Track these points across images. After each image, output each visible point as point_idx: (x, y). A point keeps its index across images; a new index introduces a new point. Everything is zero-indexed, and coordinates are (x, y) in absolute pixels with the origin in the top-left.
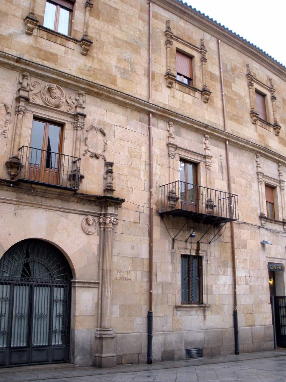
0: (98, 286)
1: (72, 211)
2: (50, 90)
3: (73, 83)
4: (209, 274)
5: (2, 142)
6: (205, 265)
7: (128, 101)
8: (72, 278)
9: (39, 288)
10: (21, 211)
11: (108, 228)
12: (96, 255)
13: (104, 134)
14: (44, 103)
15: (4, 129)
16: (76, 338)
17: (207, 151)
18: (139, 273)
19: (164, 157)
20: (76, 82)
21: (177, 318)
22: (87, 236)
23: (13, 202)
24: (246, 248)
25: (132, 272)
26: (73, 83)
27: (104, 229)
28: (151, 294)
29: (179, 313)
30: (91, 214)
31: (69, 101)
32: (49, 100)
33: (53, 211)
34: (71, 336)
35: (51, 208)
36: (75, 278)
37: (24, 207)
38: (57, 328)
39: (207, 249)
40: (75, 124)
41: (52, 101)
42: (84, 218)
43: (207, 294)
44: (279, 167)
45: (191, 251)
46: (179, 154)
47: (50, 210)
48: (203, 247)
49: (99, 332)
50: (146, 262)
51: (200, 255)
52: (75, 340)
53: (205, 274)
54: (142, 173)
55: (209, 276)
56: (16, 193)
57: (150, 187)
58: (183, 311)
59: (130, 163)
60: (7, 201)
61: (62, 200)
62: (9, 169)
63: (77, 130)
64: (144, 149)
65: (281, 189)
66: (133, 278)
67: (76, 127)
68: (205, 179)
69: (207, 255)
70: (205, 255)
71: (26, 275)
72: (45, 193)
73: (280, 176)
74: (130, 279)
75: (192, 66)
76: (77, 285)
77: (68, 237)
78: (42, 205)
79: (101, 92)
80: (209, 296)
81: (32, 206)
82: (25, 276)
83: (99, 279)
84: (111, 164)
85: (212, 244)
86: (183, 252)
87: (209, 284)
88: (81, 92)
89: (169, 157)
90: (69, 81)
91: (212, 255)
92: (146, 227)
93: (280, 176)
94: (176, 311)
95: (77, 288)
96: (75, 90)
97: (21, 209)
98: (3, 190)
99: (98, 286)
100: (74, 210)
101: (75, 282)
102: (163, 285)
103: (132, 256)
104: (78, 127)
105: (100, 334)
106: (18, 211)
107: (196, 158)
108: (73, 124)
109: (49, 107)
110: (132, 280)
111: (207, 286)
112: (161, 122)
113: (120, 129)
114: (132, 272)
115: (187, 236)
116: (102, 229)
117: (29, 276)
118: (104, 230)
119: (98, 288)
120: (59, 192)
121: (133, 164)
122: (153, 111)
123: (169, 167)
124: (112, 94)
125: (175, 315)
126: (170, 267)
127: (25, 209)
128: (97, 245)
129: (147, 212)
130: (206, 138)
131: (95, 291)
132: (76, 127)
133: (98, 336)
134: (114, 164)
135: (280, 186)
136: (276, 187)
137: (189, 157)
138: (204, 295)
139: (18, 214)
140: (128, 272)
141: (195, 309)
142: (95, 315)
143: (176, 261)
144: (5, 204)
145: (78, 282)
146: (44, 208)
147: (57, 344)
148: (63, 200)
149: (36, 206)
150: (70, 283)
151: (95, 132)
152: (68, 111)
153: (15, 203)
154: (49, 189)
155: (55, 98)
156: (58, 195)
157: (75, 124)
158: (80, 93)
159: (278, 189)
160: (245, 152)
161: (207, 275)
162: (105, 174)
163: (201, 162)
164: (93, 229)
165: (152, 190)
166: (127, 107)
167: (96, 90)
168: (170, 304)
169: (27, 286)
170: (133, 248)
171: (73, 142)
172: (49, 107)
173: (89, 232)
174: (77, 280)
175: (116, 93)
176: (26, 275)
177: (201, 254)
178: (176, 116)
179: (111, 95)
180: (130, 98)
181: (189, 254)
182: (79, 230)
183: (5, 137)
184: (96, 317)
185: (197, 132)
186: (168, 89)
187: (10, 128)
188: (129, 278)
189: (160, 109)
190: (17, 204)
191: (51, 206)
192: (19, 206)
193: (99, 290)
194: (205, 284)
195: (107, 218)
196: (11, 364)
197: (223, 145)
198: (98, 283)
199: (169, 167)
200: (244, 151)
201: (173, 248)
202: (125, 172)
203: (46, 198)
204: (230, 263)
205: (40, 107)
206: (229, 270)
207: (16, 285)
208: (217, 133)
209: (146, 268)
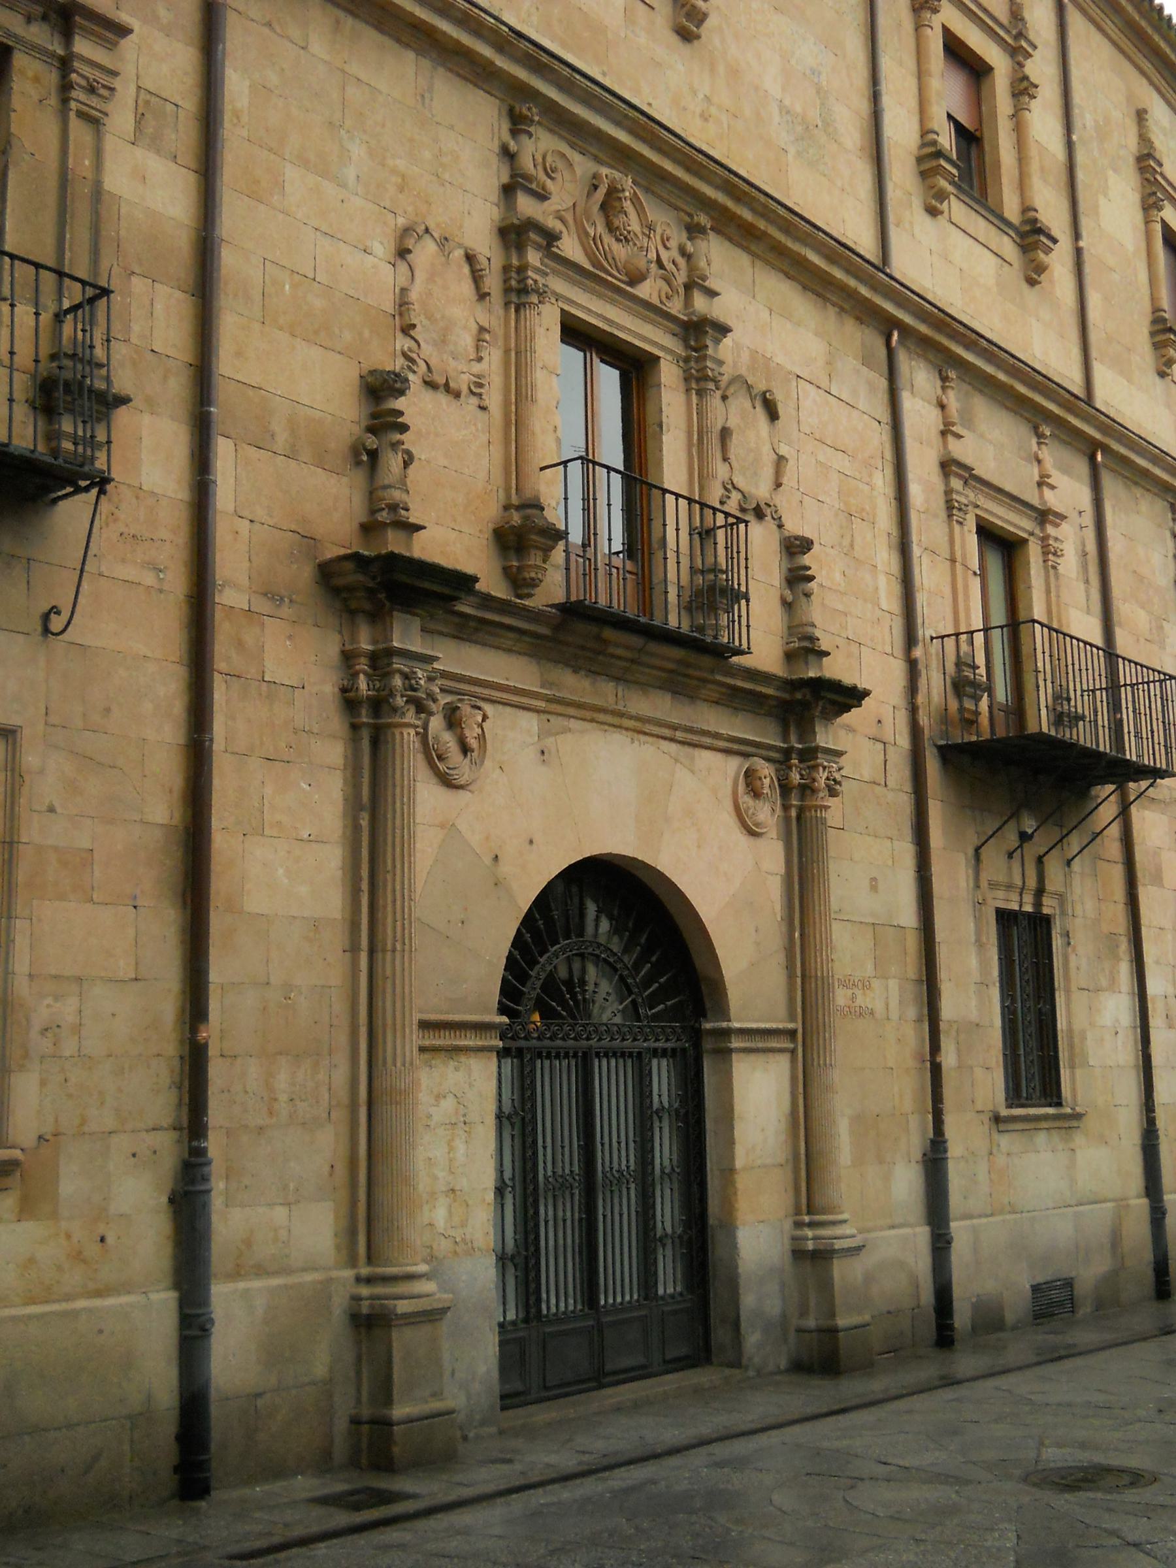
0: (792, 1046)
1: (708, 741)
2: (610, 205)
3: (679, 173)
4: (1074, 988)
5: (473, 428)
6: (1060, 950)
7: (838, 274)
8: (705, 1016)
9: (625, 1061)
10: (560, 738)
11: (816, 807)
12: (779, 919)
13: (772, 412)
14: (587, 254)
15: (477, 368)
16: (740, 1263)
17: (1046, 490)
18: (893, 984)
19: (936, 516)
20: (688, 169)
21: (1001, 1160)
22: (751, 839)
23: (505, 696)
24: (1161, 885)
25: (876, 984)
26: (679, 173)
27: (801, 810)
28: (936, 1070)
29: (1004, 1141)
30: (764, 752)
31: (665, 256)
32: (606, 247)
33: (650, 739)
34: (718, 1252)
35: (648, 728)
36: (724, 1014)
37: (565, 722)
38: (669, 1230)
39: (1063, 890)
40: (692, 364)
41: (620, 251)
42: (740, 767)
43: (1072, 1067)
44: (944, 388)
45: (1021, 895)
46: (977, 506)
47: (642, 738)
48: (1054, 882)
49: (365, 1291)
50: (912, 942)
51: (1045, 911)
52: (740, 1270)
53: (1062, 985)
54: (882, 581)
55: (1076, 995)
56: (538, 663)
57: (910, 638)
58: (1014, 1135)
59: (847, 542)
60: (515, 699)
61: (675, 693)
62: (512, 553)
63: (701, 393)
64: (882, 482)
65: (1045, 553)
66: (879, 1007)
67: (698, 380)
68: (1044, 606)
69: (1063, 913)
70: (1058, 912)
71: (564, 1013)
72: (632, 661)
73: (1045, 489)
74: (872, 1013)
75: (1149, 270)
76: (736, 1043)
77: (699, 847)
78: (621, 715)
79: (762, 224)
80: (1078, 1072)
81: (592, 720)
82: (563, 1018)
83: (792, 1017)
84: (805, 545)
85: (1076, 865)
86: (1002, 905)
87: (1077, 1026)
88: (703, 219)
89: (950, 516)
90: (669, 166)
91: (1079, 911)
92: (904, 801)
93: (1045, 489)
94: (996, 1136)
95: (734, 1056)
96: (676, 208)
97: (558, 734)
98: (498, 648)
99: (792, 1046)
100: (717, 736)
101: (727, 1033)
102: (958, 1031)
103: (871, 920)
104: (706, 378)
105: (815, 1238)
106: (552, 739)
107: (1012, 517)
108: (681, 364)
109: (610, 278)
110: (878, 1016)
111: (1070, 1031)
112: (920, 367)
113: (812, 390)
114: (876, 984)
115: (1012, 839)
116: (793, 813)
117: (574, 1017)
118: (799, 818)
119: (793, 1052)
120: (679, 662)
121: (856, 547)
122: (908, 319)
123: (953, 561)
124: (797, 239)
125: (995, 1151)
126: (973, 962)
127: (570, 730)
128: (779, 878)
129: (904, 742)
130: (1040, 436)
131: (783, 1061)
132: (698, 380)
133: (365, 1308)
134: (816, 546)
135: (1045, 539)
136: (1024, 541)
137: (1000, 518)
138: (1062, 1071)
139: (550, 753)
140: (866, 985)
141: (1044, 1125)
142: (787, 1161)
143: (988, 939)
144: (508, 709)
145: (743, 1032)
146: (627, 729)
147: (670, 1290)
148: (676, 693)
149: (601, 717)
150: (697, 1036)
151: (748, 404)
152: (661, 302)
153: (541, 704)
154: (653, 647)
155: (625, 238)
156: (671, 671)
157: (692, 364)
158: (698, 224)
159: (1034, 550)
160: (1143, 495)
161: (1068, 991)
162: (784, 584)
163: (1031, 538)
164: (767, 814)
165: (918, 652)
166: (825, 299)
167: (747, 215)
168: (980, 1108)
169: (629, 1057)
170: (874, 885)
171: (690, 445)
172: (610, 278)
173: (757, 825)
174: (736, 1025)
175: (808, 235)
176: (564, 1013)
177: (1049, 906)
178: (969, 345)
179: (790, 244)
180: (848, 259)
181: (1016, 908)
182: (728, 818)
183: (483, 408)
184: (789, 1168)
185: (1016, 413)
186: (927, 219)
187: (493, 367)
188: (870, 1007)
189: (931, 314)
190: (544, 712)
191: (604, 710)
192: (552, 718)
193: (793, 1061)
194: (1064, 1028)
195: (815, 767)
196: (546, 1388)
197: (1082, 467)
198: (792, 1034)
199: (953, 561)
200: (1138, 492)
201: (977, 886)
202: (838, 576)
203: (626, 681)
204: (1124, 946)
205: (652, 315)
206: (1125, 970)
207: (540, 1055)
208: (1077, 415)
209: (912, 967)
